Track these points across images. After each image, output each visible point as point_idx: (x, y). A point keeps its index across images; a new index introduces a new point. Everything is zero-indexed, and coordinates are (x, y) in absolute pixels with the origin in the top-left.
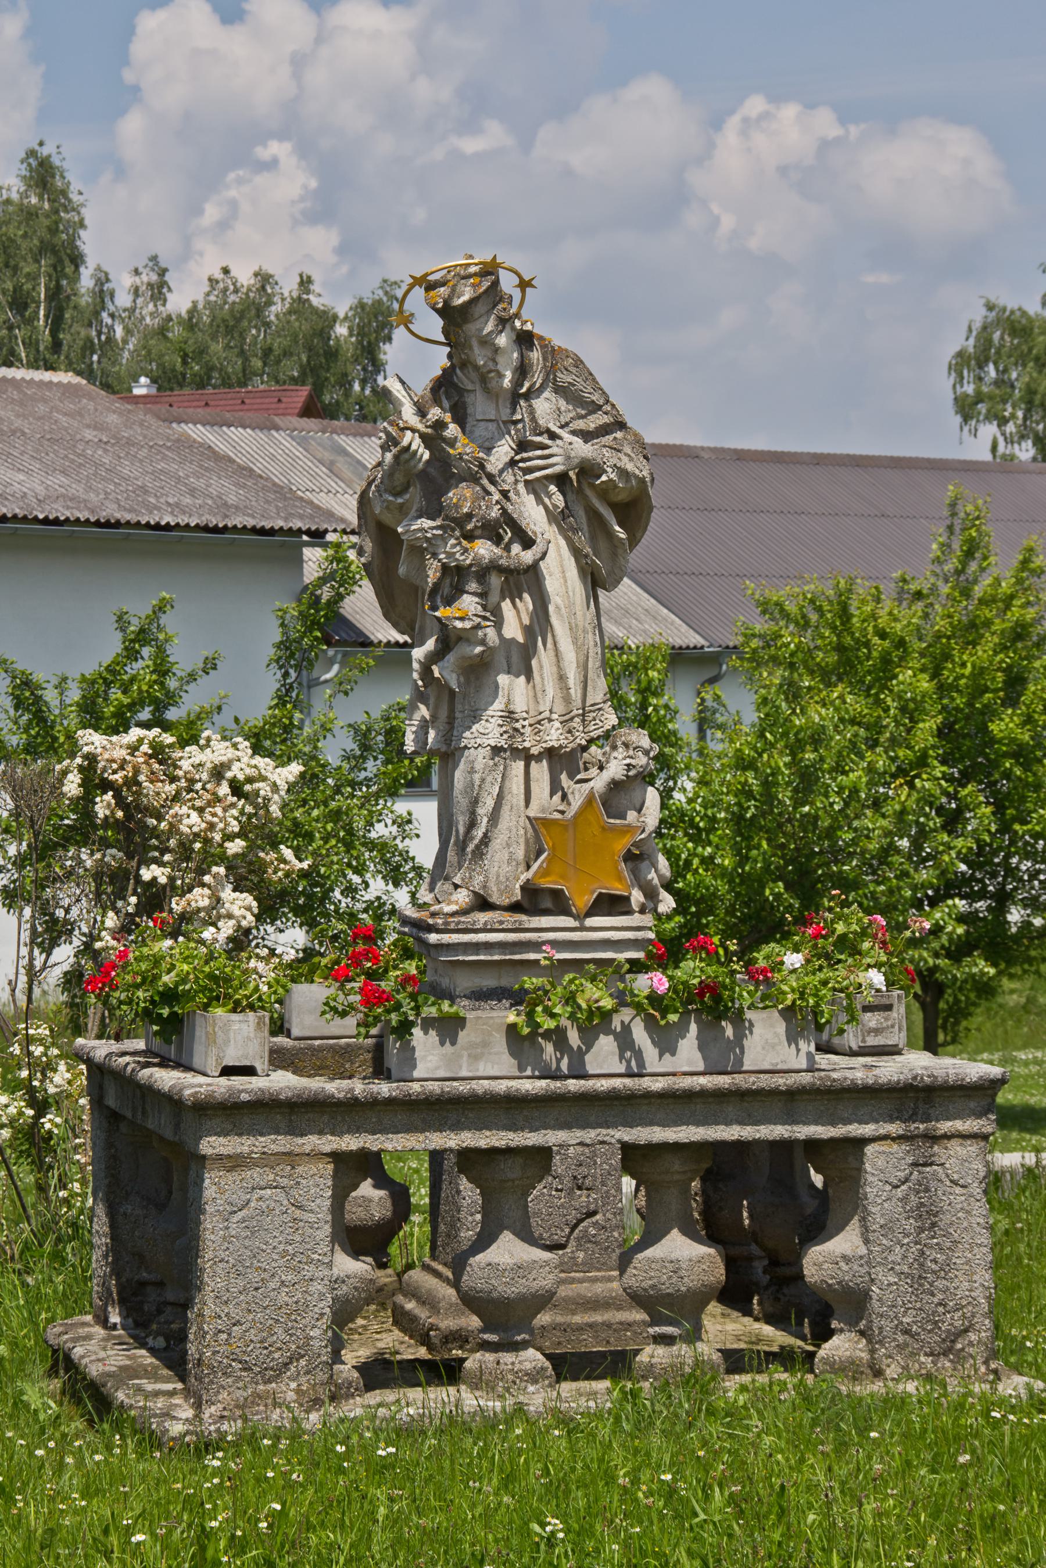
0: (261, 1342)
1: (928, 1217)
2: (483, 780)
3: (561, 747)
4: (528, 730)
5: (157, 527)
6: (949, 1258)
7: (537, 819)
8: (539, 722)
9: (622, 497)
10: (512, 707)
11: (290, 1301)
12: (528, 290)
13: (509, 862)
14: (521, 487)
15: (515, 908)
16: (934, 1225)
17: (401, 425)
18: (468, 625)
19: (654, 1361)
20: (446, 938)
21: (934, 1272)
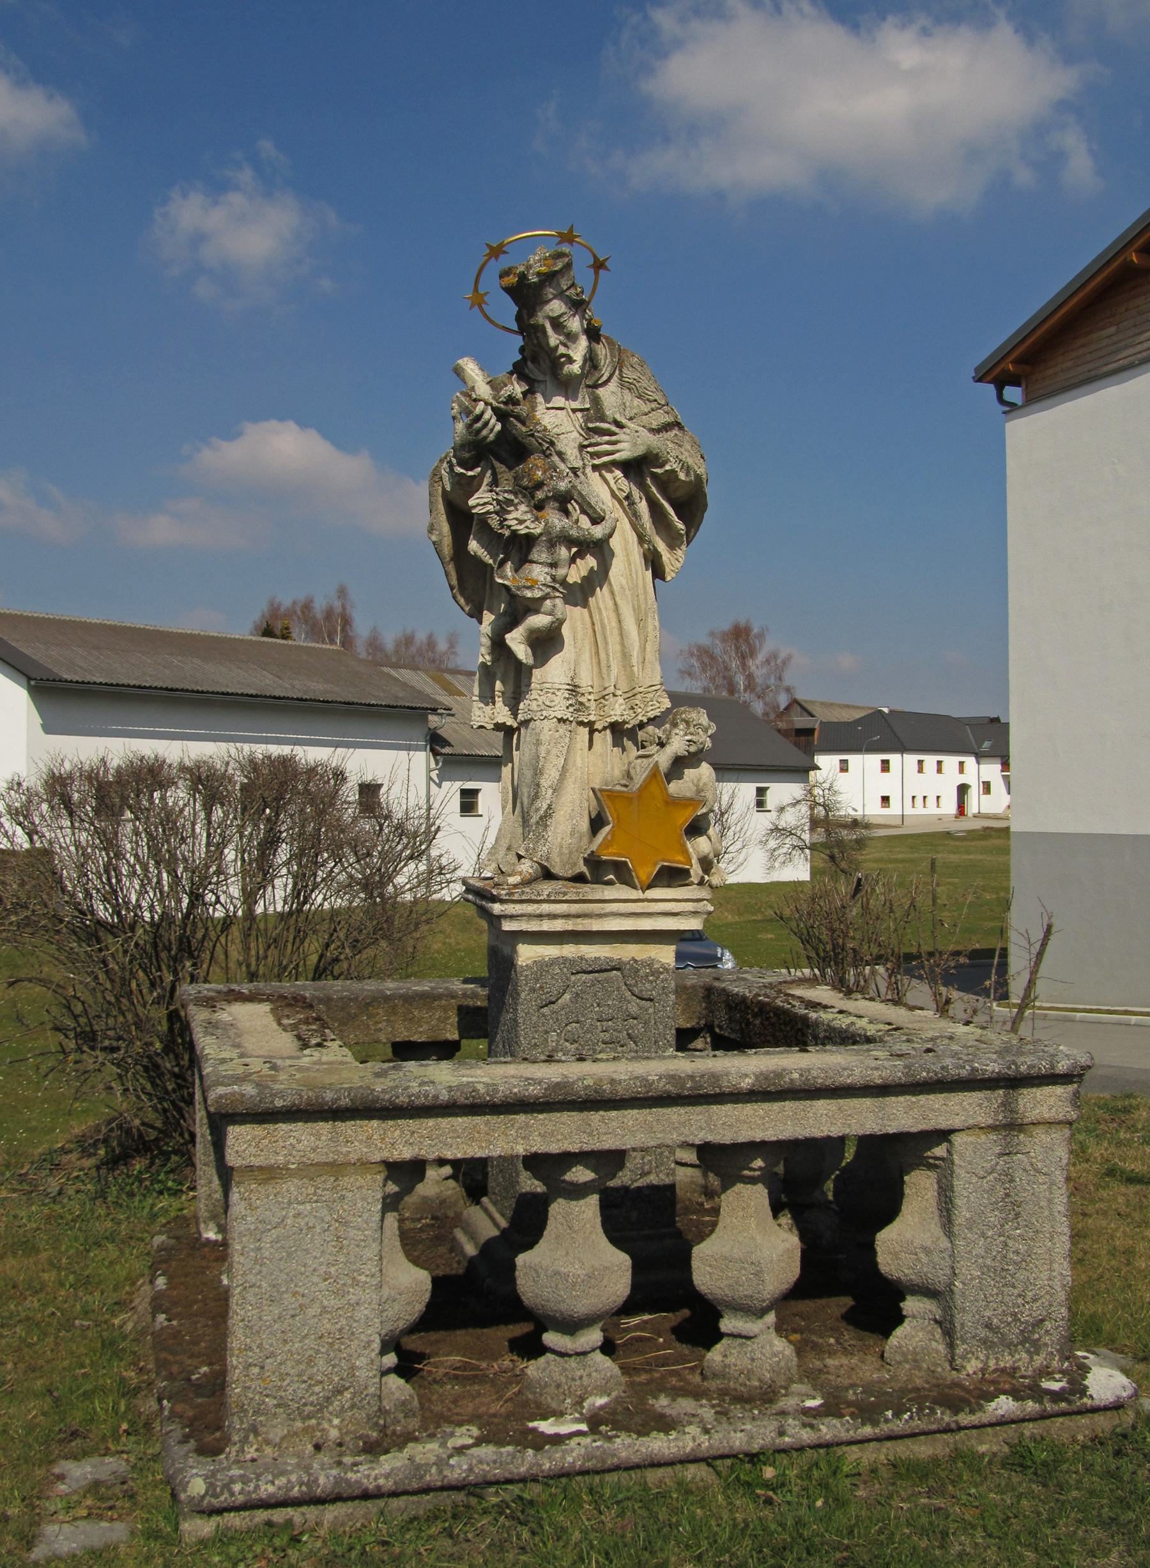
0: (299, 1375)
1: (1012, 1207)
2: (548, 752)
3: (625, 722)
4: (593, 705)
5: (369, 705)
6: (1030, 1248)
7: (601, 790)
8: (603, 697)
9: (680, 493)
10: (577, 681)
11: (333, 1329)
12: (601, 271)
13: (572, 834)
14: (589, 470)
15: (579, 879)
16: (1017, 1215)
17: (474, 396)
18: (538, 594)
19: (727, 1361)
20: (510, 909)
21: (1015, 1263)
